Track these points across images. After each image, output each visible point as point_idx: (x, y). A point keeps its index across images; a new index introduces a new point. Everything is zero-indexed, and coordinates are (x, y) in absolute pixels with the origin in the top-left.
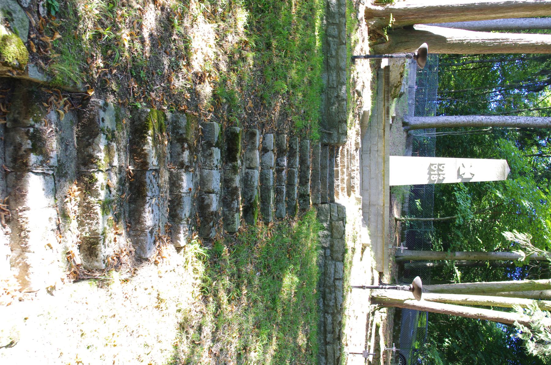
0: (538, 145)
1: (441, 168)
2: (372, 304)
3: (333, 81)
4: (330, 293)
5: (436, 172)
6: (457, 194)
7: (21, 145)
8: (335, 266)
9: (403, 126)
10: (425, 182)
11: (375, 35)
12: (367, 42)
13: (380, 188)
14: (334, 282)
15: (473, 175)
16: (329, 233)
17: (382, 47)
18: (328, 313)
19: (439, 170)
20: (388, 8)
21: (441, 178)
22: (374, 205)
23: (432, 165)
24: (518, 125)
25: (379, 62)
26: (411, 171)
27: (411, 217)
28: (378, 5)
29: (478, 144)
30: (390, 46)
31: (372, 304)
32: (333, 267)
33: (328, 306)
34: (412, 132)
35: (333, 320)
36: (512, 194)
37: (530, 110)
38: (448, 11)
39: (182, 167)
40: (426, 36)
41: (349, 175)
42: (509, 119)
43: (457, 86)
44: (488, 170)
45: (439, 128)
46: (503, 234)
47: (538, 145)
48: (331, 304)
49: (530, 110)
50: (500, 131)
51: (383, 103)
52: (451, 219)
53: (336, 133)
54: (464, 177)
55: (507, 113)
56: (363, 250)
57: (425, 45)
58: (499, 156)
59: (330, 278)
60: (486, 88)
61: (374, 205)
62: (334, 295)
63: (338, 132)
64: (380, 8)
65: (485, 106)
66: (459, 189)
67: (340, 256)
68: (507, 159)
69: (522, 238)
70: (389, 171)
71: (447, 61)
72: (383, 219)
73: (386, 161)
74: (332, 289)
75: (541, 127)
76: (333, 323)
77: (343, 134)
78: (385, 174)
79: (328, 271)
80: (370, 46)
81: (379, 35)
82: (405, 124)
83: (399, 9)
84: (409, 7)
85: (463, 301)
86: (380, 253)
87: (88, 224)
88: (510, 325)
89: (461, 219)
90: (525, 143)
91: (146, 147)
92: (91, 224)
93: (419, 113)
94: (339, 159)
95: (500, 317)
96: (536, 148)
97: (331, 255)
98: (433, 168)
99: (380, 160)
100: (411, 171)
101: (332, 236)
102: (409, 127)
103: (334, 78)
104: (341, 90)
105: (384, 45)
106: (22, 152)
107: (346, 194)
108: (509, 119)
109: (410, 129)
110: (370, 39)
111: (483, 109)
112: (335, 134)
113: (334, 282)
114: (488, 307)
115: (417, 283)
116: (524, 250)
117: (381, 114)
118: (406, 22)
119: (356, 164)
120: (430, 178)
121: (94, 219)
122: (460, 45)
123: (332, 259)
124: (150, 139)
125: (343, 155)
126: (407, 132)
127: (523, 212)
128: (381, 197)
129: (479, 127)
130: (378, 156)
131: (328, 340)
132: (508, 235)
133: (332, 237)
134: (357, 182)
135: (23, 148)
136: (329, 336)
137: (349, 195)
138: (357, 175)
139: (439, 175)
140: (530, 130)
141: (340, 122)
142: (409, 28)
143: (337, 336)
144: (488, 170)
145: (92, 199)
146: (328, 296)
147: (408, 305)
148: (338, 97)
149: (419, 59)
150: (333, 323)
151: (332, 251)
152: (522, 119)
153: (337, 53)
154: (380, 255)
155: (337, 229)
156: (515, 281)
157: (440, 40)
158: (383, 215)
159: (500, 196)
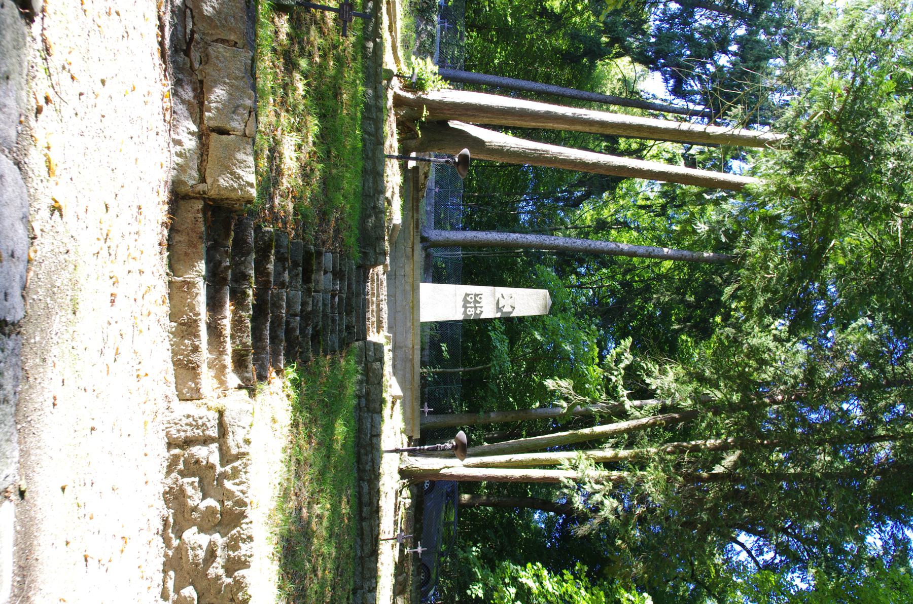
0: (578, 275)
1: (478, 299)
2: (402, 479)
3: (369, 187)
4: (366, 455)
5: (472, 305)
6: (492, 334)
7: (220, 262)
8: (372, 419)
9: (421, 242)
10: (459, 317)
11: (404, 126)
12: (396, 137)
13: (409, 324)
14: (371, 439)
15: (513, 308)
16: (365, 378)
17: (413, 143)
18: (364, 480)
19: (476, 302)
20: (420, 97)
21: (478, 312)
22: (401, 348)
23: (467, 295)
24: (556, 247)
25: (406, 163)
26: (442, 302)
27: (435, 368)
28: (408, 92)
29: (509, 270)
30: (422, 144)
31: (402, 479)
32: (370, 420)
33: (364, 471)
34: (432, 250)
35: (370, 489)
36: (553, 333)
37: (567, 228)
38: (487, 112)
39: (283, 287)
40: (464, 138)
41: (378, 306)
42: (546, 239)
43: (480, 189)
44: (527, 302)
45: (466, 246)
46: (545, 383)
47: (578, 275)
48: (368, 468)
49: (567, 228)
50: (535, 255)
51: (411, 214)
52: (485, 369)
53: (372, 252)
54: (505, 310)
55: (540, 232)
56: (393, 403)
57: (466, 151)
58: (539, 285)
59: (366, 435)
60: (517, 194)
61: (401, 348)
62: (370, 456)
63: (375, 251)
64: (410, 95)
65: (516, 219)
66: (494, 329)
67: (377, 406)
68: (549, 289)
69: (565, 385)
70: (419, 302)
71: (486, 169)
72: (413, 365)
73: (415, 290)
74: (369, 449)
75: (579, 251)
76: (369, 493)
77: (380, 254)
78: (415, 306)
79: (364, 427)
80: (399, 141)
81: (408, 128)
82: (424, 240)
83: (433, 101)
84: (445, 100)
85: (507, 462)
86: (409, 410)
87: (239, 337)
88: (554, 483)
89: (497, 368)
90: (564, 271)
91: (269, 266)
92: (242, 337)
93: (439, 224)
94: (369, 284)
95: (546, 476)
96: (573, 276)
97: (367, 406)
98: (468, 299)
99: (408, 288)
100: (442, 302)
101: (367, 382)
102: (428, 244)
103: (371, 185)
104: (378, 200)
105: (415, 141)
106: (222, 268)
107: (375, 330)
108: (546, 239)
109: (429, 247)
110: (399, 134)
111: (509, 223)
112: (372, 253)
113: (371, 439)
114: (534, 467)
115: (461, 438)
116: (566, 399)
117: (409, 228)
118: (441, 117)
119: (384, 291)
120: (465, 312)
121: (244, 332)
122: (500, 151)
123: (369, 411)
124: (272, 258)
125: (373, 281)
126: (426, 250)
127: (565, 357)
128: (410, 336)
129: (509, 247)
130: (406, 282)
131: (364, 515)
132: (550, 383)
133: (367, 383)
134: (385, 315)
135: (224, 264)
136: (365, 509)
137: (378, 332)
138: (384, 307)
139: (476, 308)
140: (568, 256)
141: (377, 238)
142: (443, 124)
143: (375, 509)
144: (527, 302)
145: (243, 313)
146: (364, 458)
147: (444, 475)
148: (375, 207)
149: (460, 167)
150: (369, 493)
151: (367, 400)
152: (559, 239)
153: (374, 154)
154: (409, 414)
155: (374, 373)
156: (560, 434)
157: (477, 143)
158: (412, 360)
159: (539, 338)
